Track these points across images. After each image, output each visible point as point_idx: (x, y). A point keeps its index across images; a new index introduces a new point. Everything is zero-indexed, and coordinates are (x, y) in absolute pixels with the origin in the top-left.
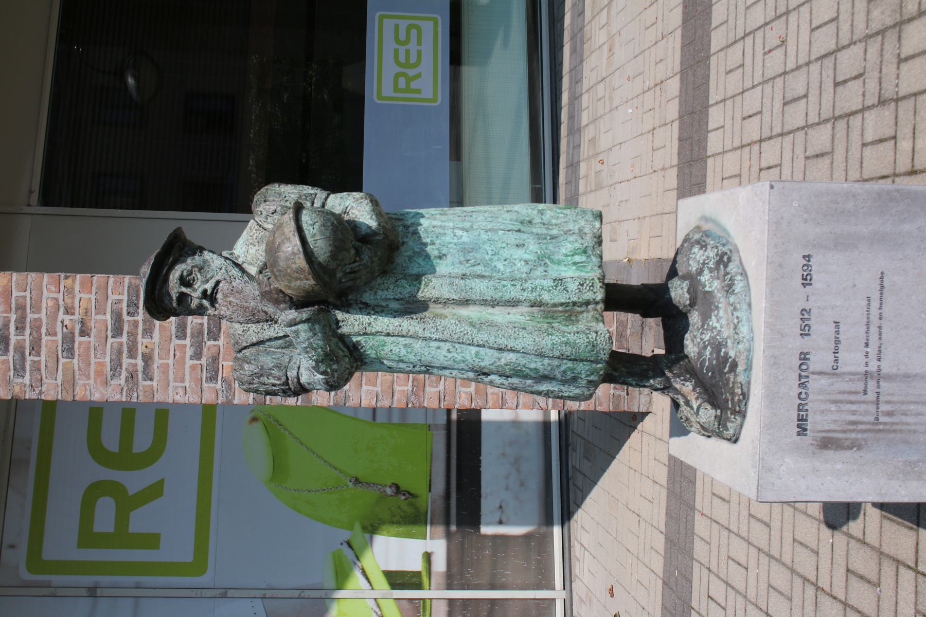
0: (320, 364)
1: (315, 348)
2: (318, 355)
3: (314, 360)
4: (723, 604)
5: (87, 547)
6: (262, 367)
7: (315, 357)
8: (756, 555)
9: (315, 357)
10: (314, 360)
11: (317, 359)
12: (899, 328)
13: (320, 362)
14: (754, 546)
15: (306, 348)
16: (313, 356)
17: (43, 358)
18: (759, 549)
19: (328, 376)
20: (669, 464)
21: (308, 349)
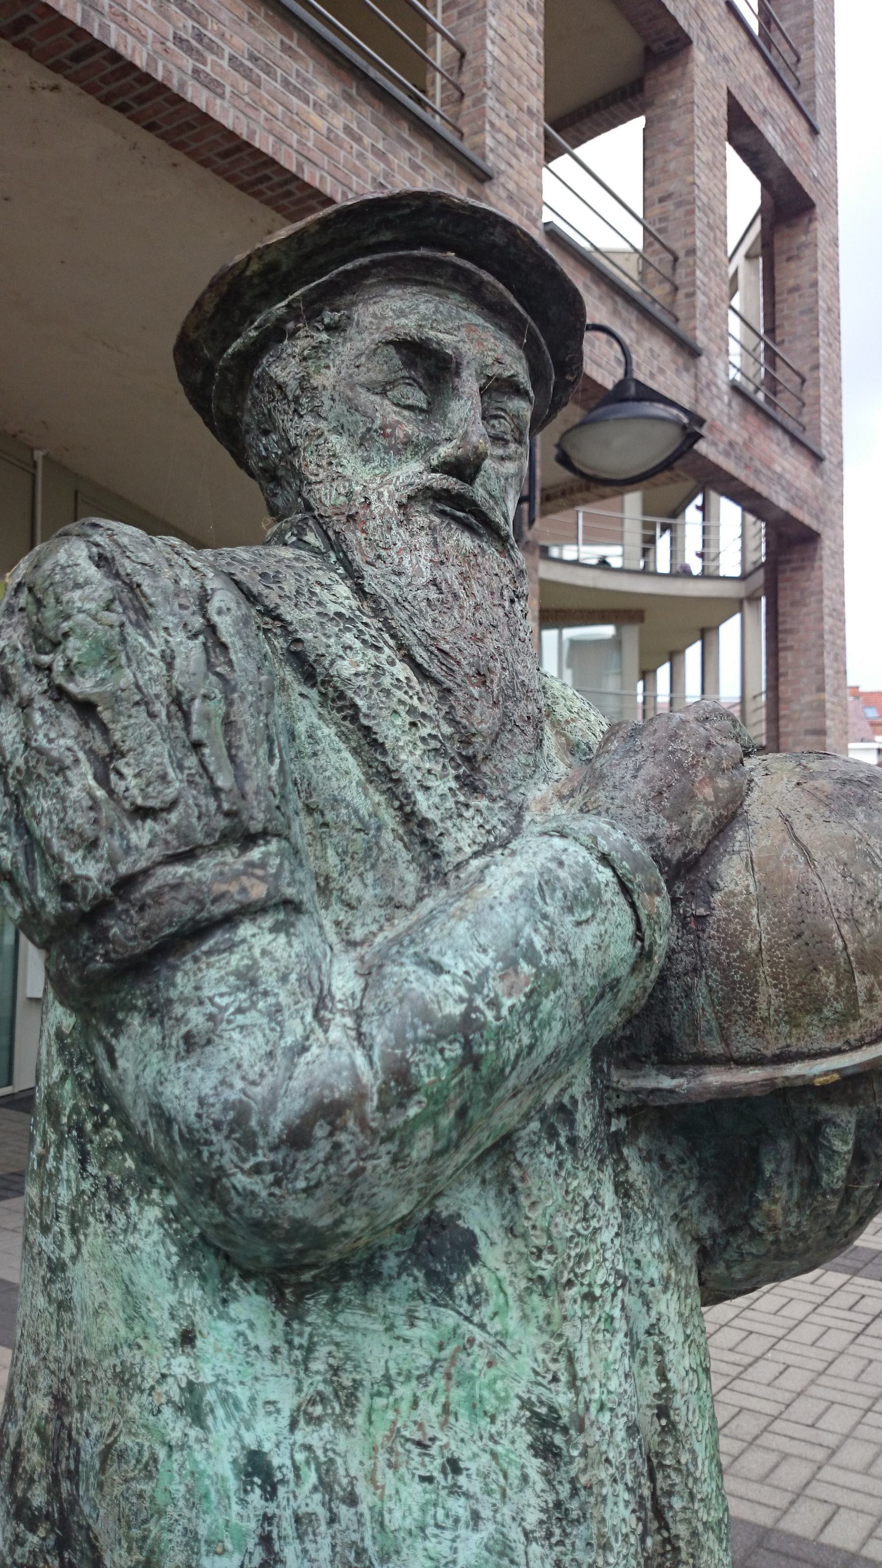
0: (455, 1051)
1: (535, 1008)
2: (503, 1033)
3: (471, 1008)
4: (781, 1313)
5: (808, 529)
6: (461, 1183)
7: (490, 1015)
8: (771, 1436)
9: (490, 1015)
10: (471, 1008)
11: (482, 1026)
12: (668, 1548)
13: (467, 1045)
14: (793, 1401)
15: (531, 956)
16: (494, 1004)
17: (6, 599)
18: (788, 1406)
19: (383, 1108)
20: (822, 1546)
21: (526, 968)
